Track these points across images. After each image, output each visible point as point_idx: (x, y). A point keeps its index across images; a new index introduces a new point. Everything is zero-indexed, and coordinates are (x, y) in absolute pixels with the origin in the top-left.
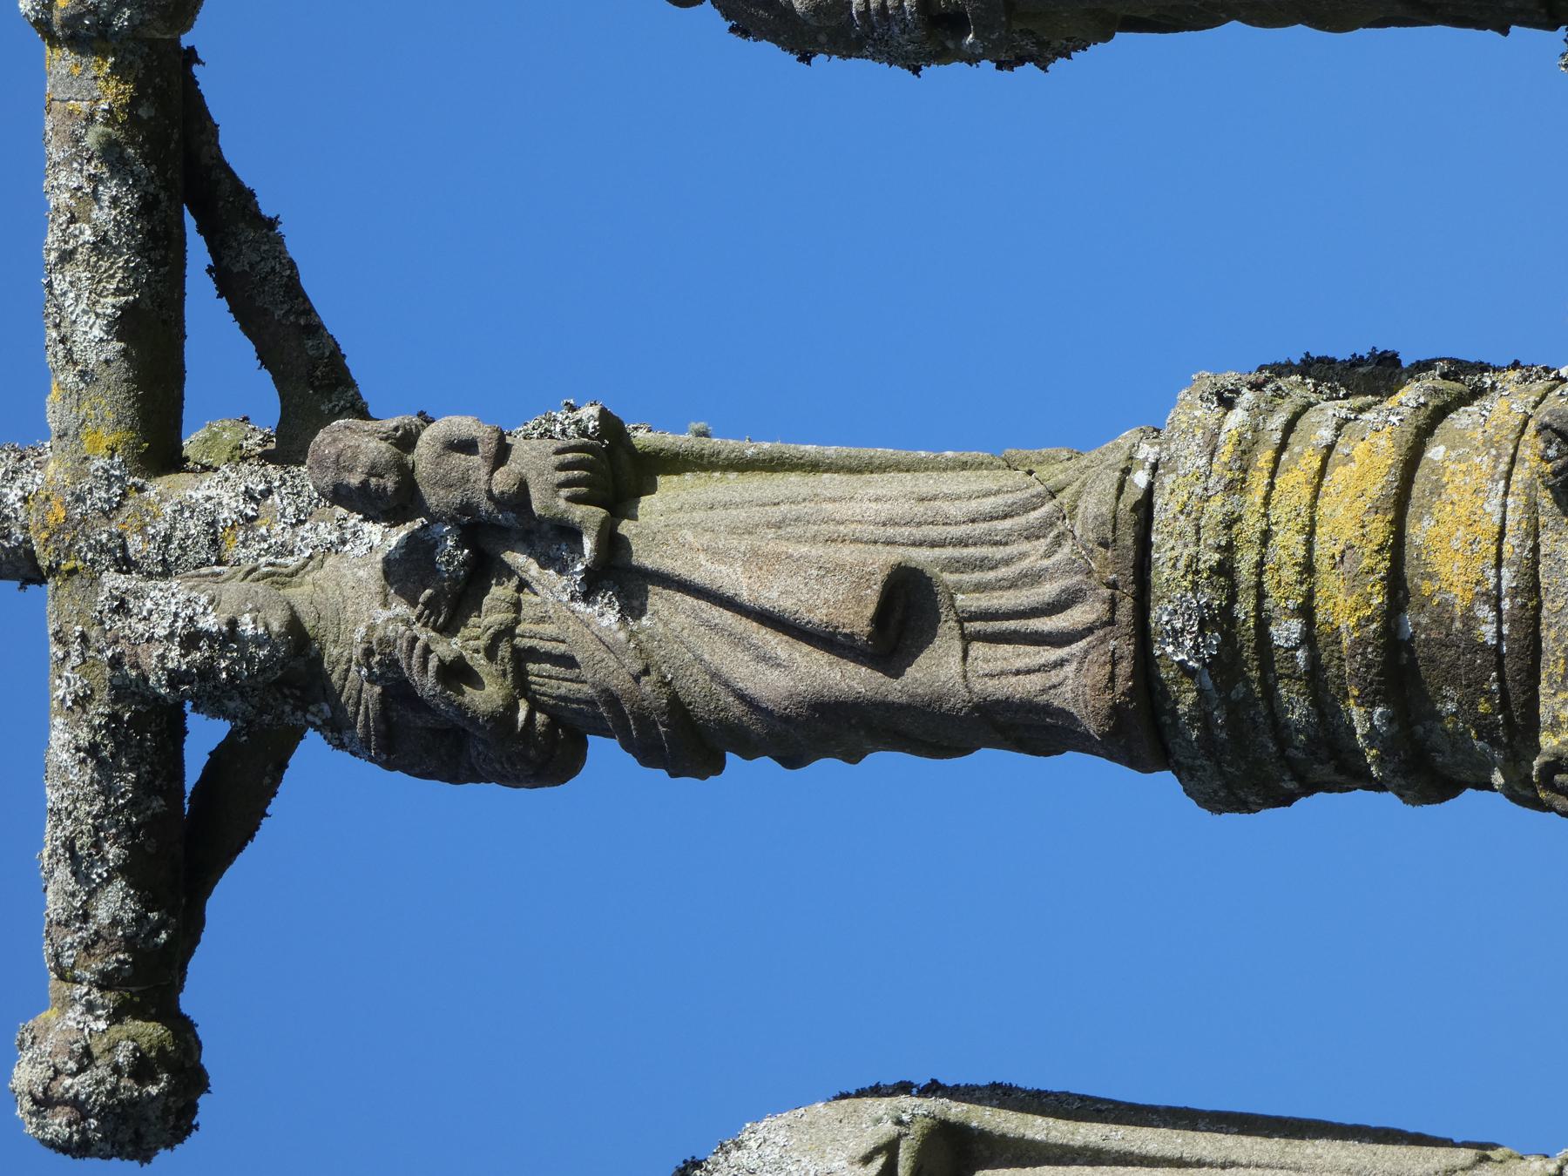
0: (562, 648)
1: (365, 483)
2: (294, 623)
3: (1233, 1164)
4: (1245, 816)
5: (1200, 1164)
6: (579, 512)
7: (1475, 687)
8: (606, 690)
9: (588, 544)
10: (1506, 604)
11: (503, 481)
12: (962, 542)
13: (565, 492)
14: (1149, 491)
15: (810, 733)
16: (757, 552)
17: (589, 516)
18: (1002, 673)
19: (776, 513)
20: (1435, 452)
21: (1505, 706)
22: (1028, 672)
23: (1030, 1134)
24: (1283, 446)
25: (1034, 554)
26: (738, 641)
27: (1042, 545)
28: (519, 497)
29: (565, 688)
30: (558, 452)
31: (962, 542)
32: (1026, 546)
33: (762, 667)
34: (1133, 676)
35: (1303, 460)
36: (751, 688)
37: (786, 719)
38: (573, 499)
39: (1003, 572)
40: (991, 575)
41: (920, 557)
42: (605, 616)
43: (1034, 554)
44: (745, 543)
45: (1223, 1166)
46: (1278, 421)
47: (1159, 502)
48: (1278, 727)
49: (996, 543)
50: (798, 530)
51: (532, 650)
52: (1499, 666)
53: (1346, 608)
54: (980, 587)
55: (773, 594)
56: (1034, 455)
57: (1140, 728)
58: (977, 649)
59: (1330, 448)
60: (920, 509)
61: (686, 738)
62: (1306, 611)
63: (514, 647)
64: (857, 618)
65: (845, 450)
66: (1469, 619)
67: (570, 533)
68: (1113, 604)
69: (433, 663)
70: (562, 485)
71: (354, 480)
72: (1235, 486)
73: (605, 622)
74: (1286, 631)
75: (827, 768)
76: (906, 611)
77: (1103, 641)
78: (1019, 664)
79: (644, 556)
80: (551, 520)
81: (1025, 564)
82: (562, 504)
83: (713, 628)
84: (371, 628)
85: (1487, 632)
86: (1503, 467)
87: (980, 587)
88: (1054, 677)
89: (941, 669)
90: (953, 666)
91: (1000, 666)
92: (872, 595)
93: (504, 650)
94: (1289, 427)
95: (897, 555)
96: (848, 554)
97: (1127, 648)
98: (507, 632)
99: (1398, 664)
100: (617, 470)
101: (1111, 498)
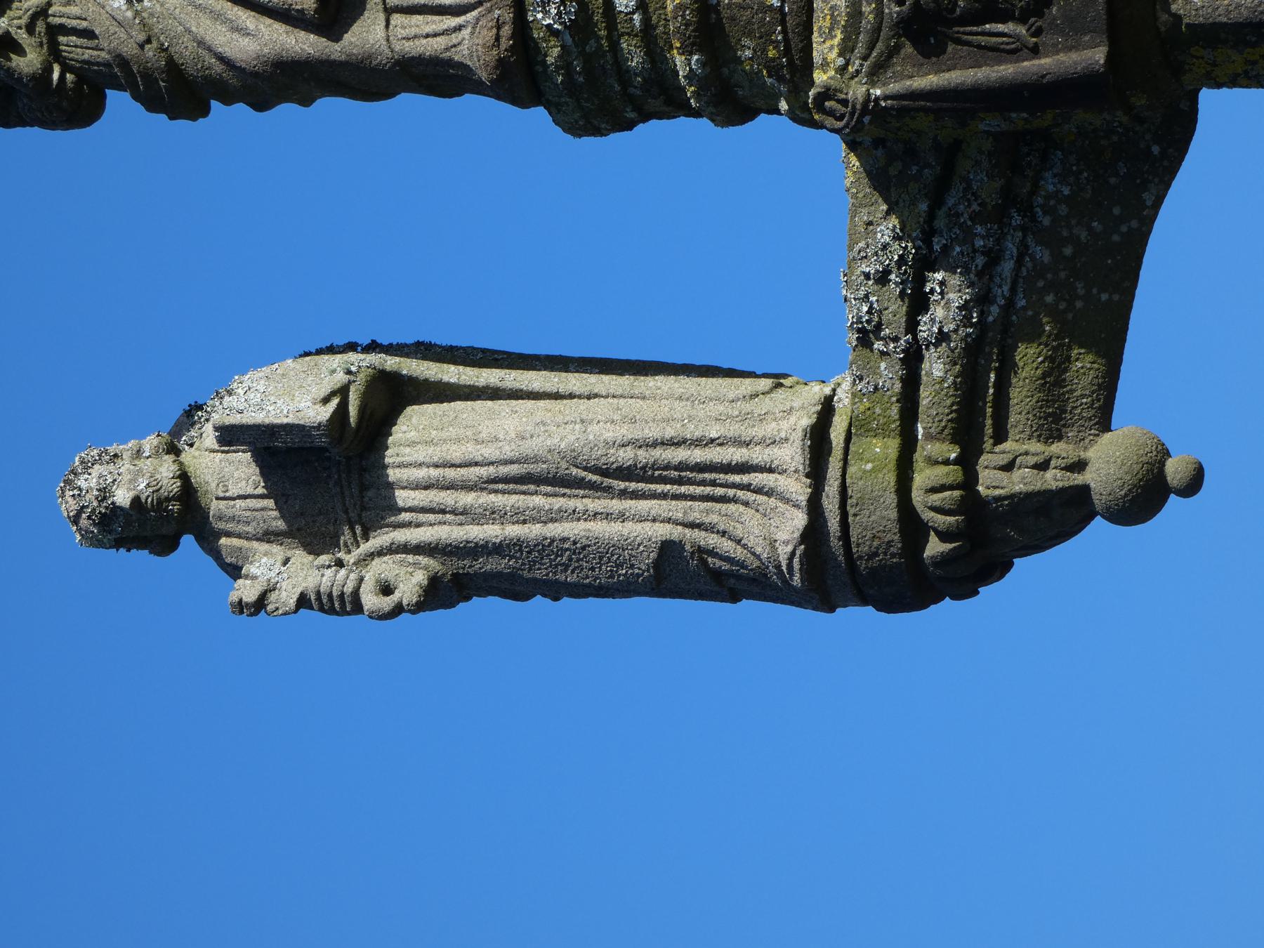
0: (84, 24)
3: (596, 396)
5: (571, 396)
18: (415, 37)
21: (787, 52)
22: (435, 35)
23: (446, 378)
33: (236, 36)
34: (512, 37)
36: (228, 51)
37: (255, 75)
45: (589, 398)
51: (62, 26)
52: (783, 22)
78: (428, 29)
88: (455, 38)
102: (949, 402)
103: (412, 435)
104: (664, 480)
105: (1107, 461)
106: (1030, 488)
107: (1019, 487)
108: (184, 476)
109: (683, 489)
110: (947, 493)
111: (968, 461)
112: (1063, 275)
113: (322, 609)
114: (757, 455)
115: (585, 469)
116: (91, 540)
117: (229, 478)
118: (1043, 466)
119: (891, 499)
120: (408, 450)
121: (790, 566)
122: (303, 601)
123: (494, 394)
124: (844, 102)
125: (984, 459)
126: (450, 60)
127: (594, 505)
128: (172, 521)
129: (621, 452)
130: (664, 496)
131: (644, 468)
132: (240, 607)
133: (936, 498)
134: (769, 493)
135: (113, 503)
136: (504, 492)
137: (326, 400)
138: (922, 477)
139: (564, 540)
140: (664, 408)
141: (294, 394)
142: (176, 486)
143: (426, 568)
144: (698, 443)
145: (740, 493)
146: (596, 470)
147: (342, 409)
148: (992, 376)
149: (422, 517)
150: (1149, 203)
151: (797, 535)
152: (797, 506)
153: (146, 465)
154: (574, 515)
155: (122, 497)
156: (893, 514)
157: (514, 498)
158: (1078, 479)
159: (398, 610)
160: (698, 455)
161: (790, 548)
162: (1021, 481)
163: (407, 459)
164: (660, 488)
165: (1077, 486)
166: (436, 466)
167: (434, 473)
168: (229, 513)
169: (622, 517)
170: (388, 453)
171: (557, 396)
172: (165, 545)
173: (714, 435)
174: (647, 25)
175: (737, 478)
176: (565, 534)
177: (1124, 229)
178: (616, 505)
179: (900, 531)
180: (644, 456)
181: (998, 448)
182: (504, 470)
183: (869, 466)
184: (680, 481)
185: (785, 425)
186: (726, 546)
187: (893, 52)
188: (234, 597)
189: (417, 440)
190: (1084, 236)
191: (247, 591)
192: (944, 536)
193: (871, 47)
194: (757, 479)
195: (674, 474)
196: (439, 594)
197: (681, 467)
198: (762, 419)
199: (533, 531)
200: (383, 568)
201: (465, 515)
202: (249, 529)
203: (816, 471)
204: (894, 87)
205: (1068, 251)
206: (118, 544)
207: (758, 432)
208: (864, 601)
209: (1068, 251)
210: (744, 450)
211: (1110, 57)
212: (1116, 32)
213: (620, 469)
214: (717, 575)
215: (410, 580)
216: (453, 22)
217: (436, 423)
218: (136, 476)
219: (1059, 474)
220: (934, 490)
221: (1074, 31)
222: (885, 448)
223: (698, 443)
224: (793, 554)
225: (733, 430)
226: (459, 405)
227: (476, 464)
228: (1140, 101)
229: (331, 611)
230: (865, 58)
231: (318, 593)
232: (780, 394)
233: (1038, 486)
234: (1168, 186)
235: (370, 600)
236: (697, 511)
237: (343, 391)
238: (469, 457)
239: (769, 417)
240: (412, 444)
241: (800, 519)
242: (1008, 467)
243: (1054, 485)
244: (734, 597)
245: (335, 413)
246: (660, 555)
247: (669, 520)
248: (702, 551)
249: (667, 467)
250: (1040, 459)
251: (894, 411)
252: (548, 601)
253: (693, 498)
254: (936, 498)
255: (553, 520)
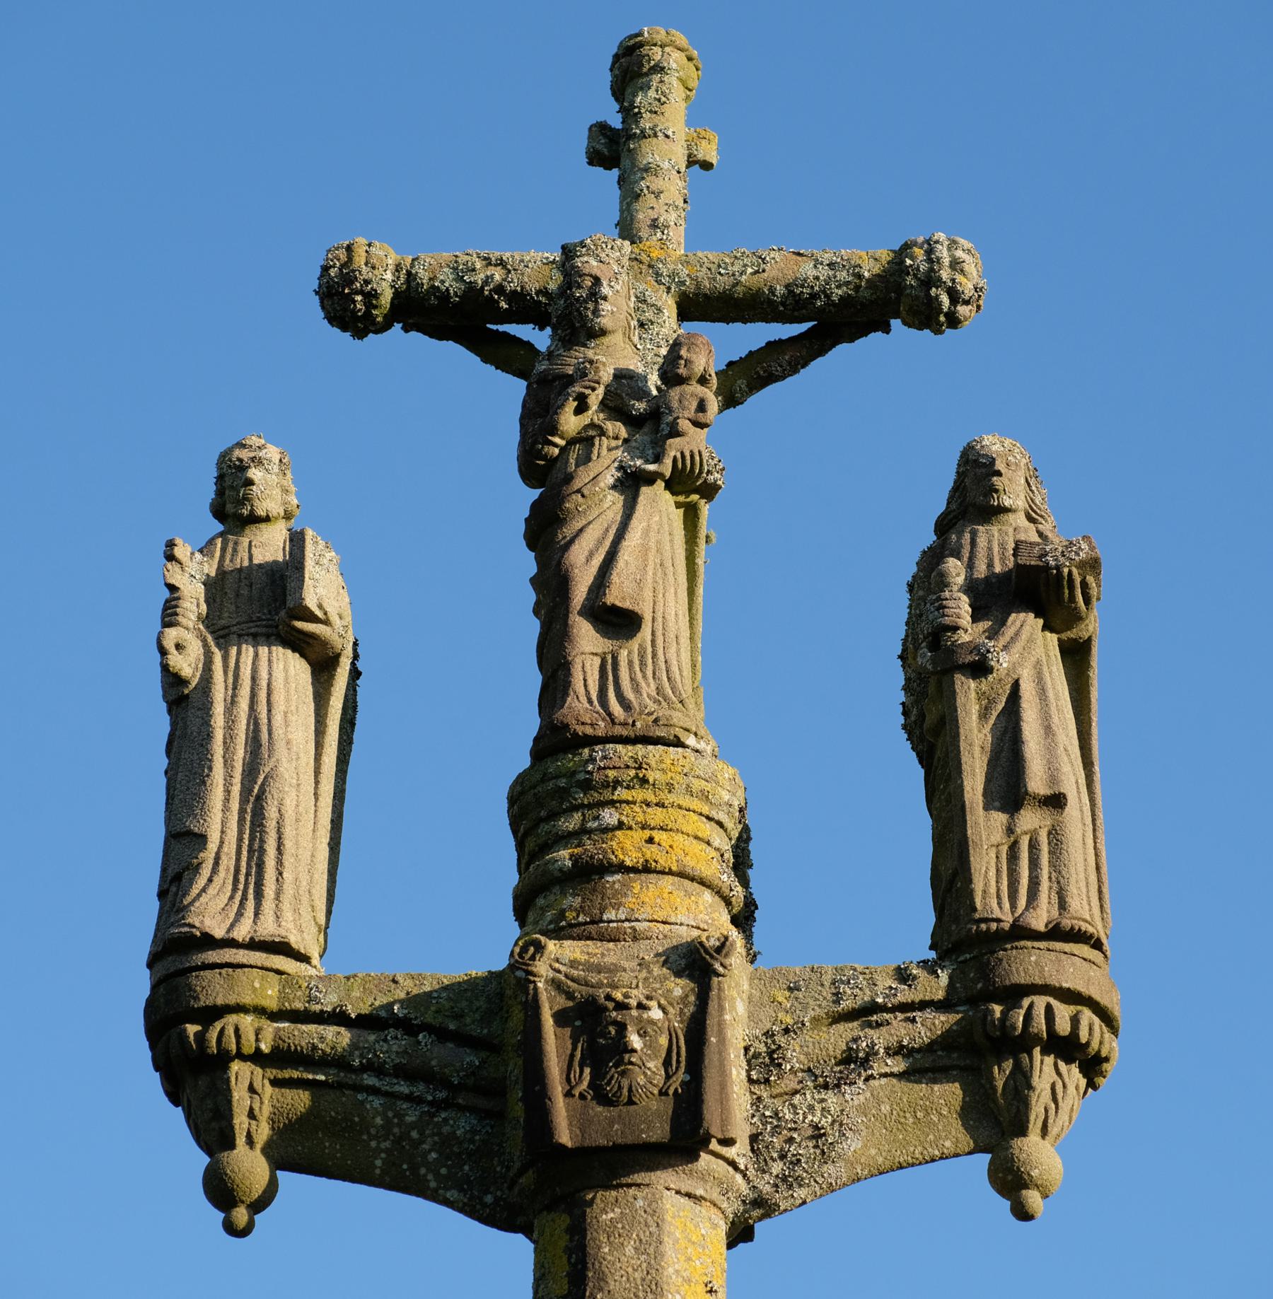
0: (595, 458)
1: (680, 357)
2: (603, 332)
3: (317, 799)
4: (518, 411)
5: (317, 783)
6: (668, 462)
7: (581, 910)
8: (572, 478)
9: (652, 467)
10: (627, 924)
11: (684, 425)
12: (654, 655)
13: (679, 455)
14: (683, 746)
15: (551, 586)
16: (645, 548)
17: (667, 468)
18: (584, 672)
19: (668, 564)
20: (708, 896)
21: (571, 926)
22: (585, 686)
23: (333, 699)
24: (709, 818)
25: (649, 688)
26: (600, 542)
27: (654, 694)
28: (675, 433)
29: (572, 461)
30: (700, 452)
31: (654, 655)
32: (653, 686)
33: (586, 553)
34: (585, 735)
35: (707, 830)
36: (575, 548)
37: (559, 563)
38: (675, 459)
39: (639, 675)
40: (637, 668)
41: (646, 632)
42: (609, 478)
43: (649, 688)
44: (652, 544)
45: (315, 794)
46: (722, 816)
47: (680, 750)
48: (554, 816)
49: (654, 673)
50: (659, 574)
51: (593, 445)
52: (593, 922)
53: (628, 847)
54: (630, 663)
55: (626, 556)
56: (701, 700)
57: (555, 741)
58: (597, 661)
59: (708, 843)
60: (672, 636)
61: (546, 531)
62: (621, 825)
63: (593, 437)
64: (614, 597)
65: (701, 608)
66: (617, 906)
67: (657, 459)
68: (625, 724)
69: (587, 392)
70: (682, 453)
71: (683, 352)
72: (689, 791)
73: (609, 477)
74: (610, 816)
75: (530, 597)
76: (618, 623)
77: (603, 720)
78: (590, 682)
79: (645, 491)
80: (665, 449)
81: (643, 684)
82: (672, 454)
83: (607, 530)
84: (604, 364)
85: (610, 914)
86: (702, 926)
87: (630, 663)
88: (583, 699)
89: (587, 641)
90: (588, 648)
91: (589, 674)
92: (627, 605)
93: (591, 433)
94: (720, 824)
95: (648, 617)
96: (648, 594)
97: (600, 733)
98: (602, 433)
99: (590, 872)
100: (690, 484)
101: (681, 724)
102: (303, 1044)
103: (292, 671)
104: (252, 840)
105: (250, 1166)
106: (235, 1104)
107: (236, 1095)
108: (267, 519)
109: (245, 853)
110: (234, 1040)
111: (257, 1058)
112: (396, 1130)
113: (167, 601)
114: (268, 904)
115: (263, 784)
116: (224, 457)
117: (268, 545)
118: (251, 1115)
119: (232, 1000)
120: (281, 666)
121: (185, 925)
122: (172, 588)
123: (319, 746)
124: (533, 958)
125: (259, 1071)
126: (568, 695)
127: (236, 789)
128: (232, 506)
129: (274, 809)
130: (240, 840)
131: (262, 825)
132: (171, 544)
133: (230, 1031)
134: (239, 914)
135: (249, 467)
136: (247, 729)
137: (320, 607)
138: (247, 1022)
139: (210, 769)
140: (305, 843)
141: (324, 588)
142: (261, 512)
143: (194, 675)
144: (280, 862)
145: (240, 893)
146: (262, 790)
147: (313, 618)
148: (323, 1078)
149: (231, 674)
150: (448, 1195)
151: (207, 930)
152: (228, 931)
153: (277, 492)
154: (228, 777)
155: (255, 473)
156: (220, 1001)
157: (244, 737)
158: (241, 1140)
159: (163, 652)
160: (270, 863)
161: (197, 924)
162: (240, 1096)
163: (275, 666)
164: (246, 836)
165: (235, 1140)
166: (268, 685)
167: (264, 684)
168: (240, 548)
169: (226, 809)
170: (280, 649)
171: (317, 772)
172: (219, 512)
173: (285, 875)
174: (590, 832)
175: (251, 891)
176: (215, 769)
177: (430, 1177)
178: (235, 805)
179: (207, 1006)
180: (271, 825)
181: (267, 1082)
182: (264, 729)
183: (257, 985)
184: (251, 851)
185: (291, 926)
186: (201, 882)
187: (570, 995)
188: (178, 541)
189: (288, 671)
190: (426, 1146)
191: (181, 551)
192: (201, 1037)
193: (573, 980)
194: (250, 904)
195: (256, 846)
196: (172, 680)
197: (262, 851)
198: (296, 911)
199: (218, 720)
200: (195, 649)
201: (232, 703)
202: (227, 562)
203: (255, 945)
204: (544, 997)
205: (414, 1134)
206: (220, 478)
207: (286, 906)
208: (154, 988)
209: (414, 1134)
210: (273, 896)
211: (563, 1146)
212: (583, 1154)
213: (262, 808)
214: (178, 878)
215: (187, 665)
216: (594, 698)
217: (300, 688)
218: (270, 489)
219: (245, 1126)
220: (237, 1030)
221: (581, 1122)
222: (270, 995)
223: (280, 862)
224: (194, 927)
225: (289, 889)
226: (312, 706)
227: (269, 711)
228: (527, 1180)
229: (165, 609)
230: (566, 976)
231: (179, 598)
232: (314, 930)
233: (236, 1110)
234: (461, 1210)
235: (172, 635)
236: (228, 862)
237: (326, 622)
238: (275, 705)
239: (297, 916)
240: (286, 670)
241: (219, 933)
242: (252, 1089)
243: (236, 1121)
244: (162, 894)
245: (312, 613)
246: (196, 835)
247: (222, 842)
248: (197, 869)
249: (262, 841)
250: (257, 1112)
251: (299, 1005)
252: (165, 767)
253: (238, 860)
254: (230, 1031)
255: (225, 762)
